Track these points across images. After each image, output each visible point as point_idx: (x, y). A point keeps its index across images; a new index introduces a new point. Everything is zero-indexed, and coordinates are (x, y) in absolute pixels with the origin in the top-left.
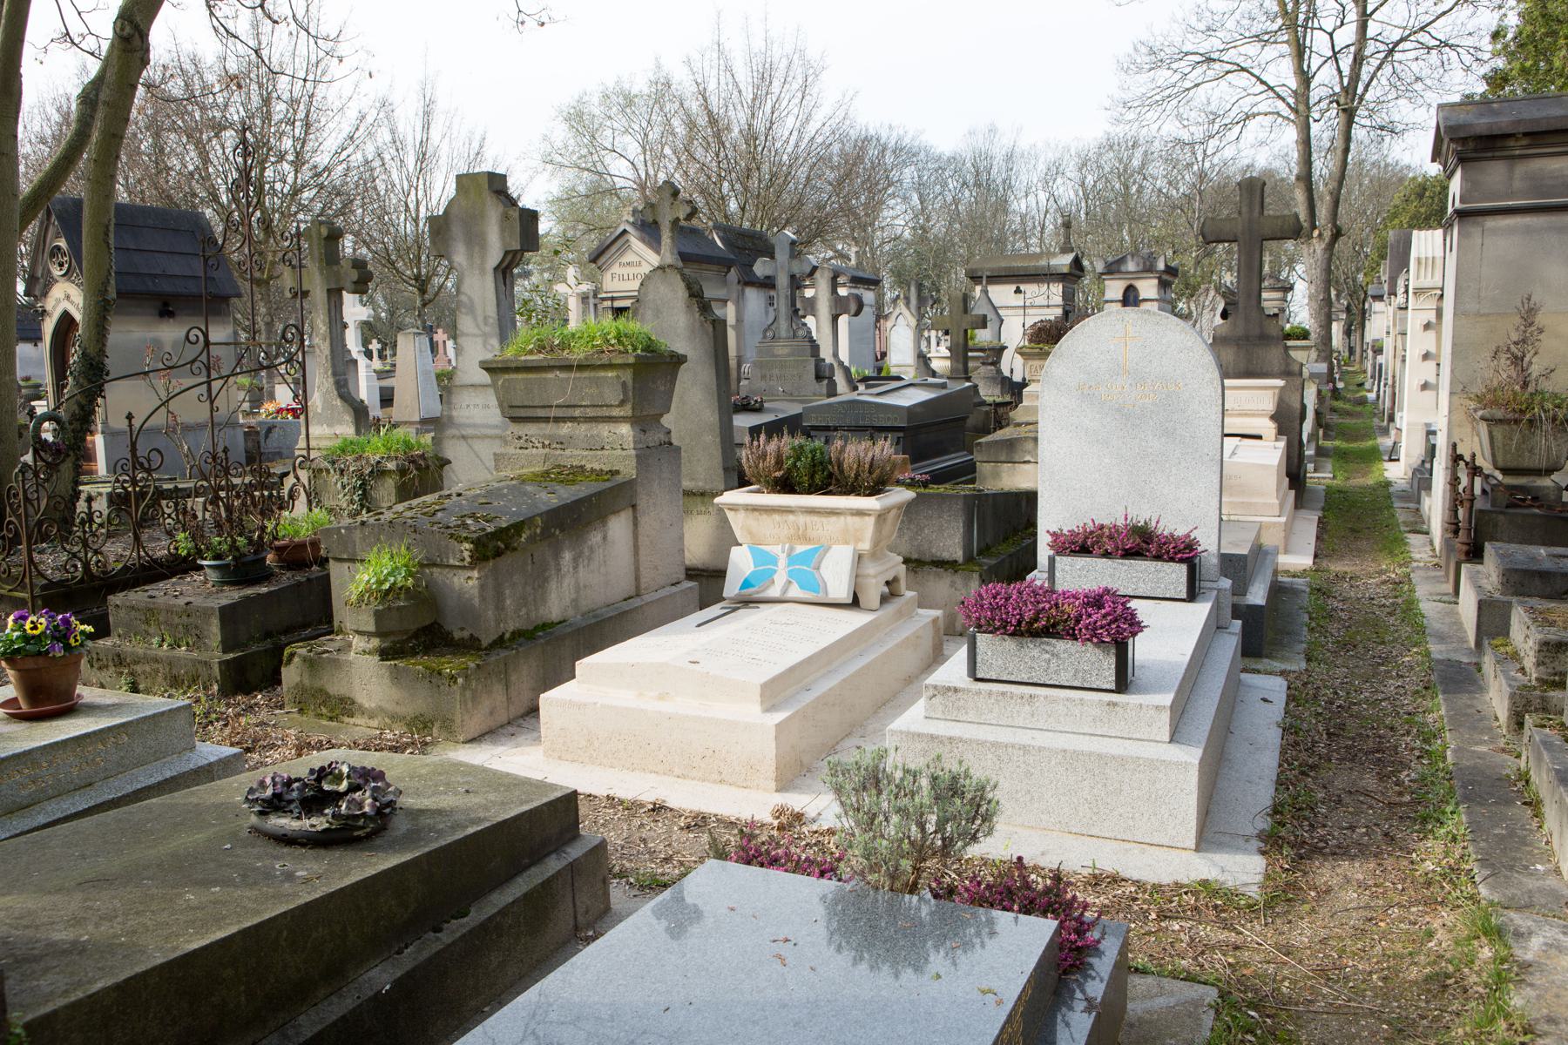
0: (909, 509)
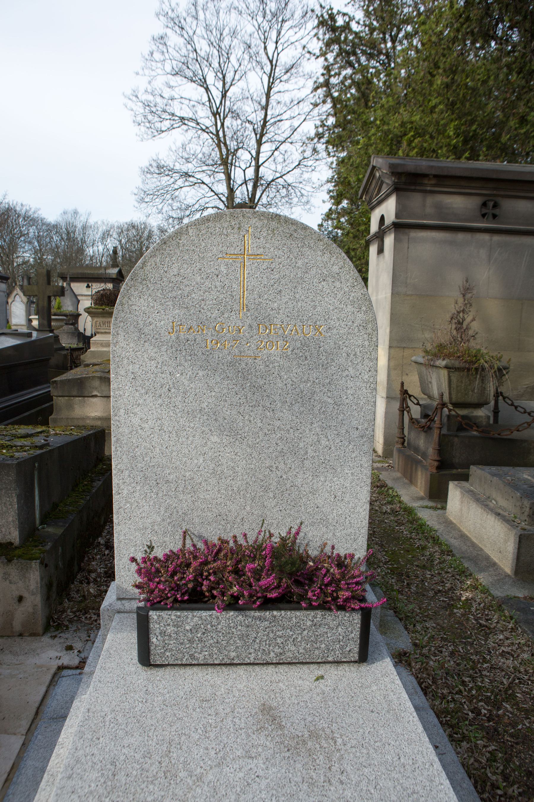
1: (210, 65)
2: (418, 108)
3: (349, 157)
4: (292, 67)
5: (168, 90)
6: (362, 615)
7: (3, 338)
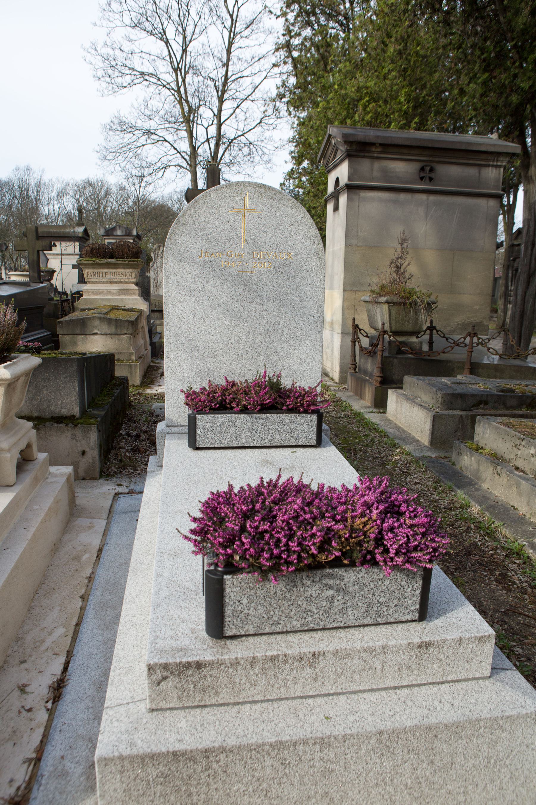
0: (36, 371)
1: (170, 18)
2: (373, 74)
3: (310, 118)
4: (252, 23)
5: (129, 44)
6: (318, 416)
7: (5, 287)
